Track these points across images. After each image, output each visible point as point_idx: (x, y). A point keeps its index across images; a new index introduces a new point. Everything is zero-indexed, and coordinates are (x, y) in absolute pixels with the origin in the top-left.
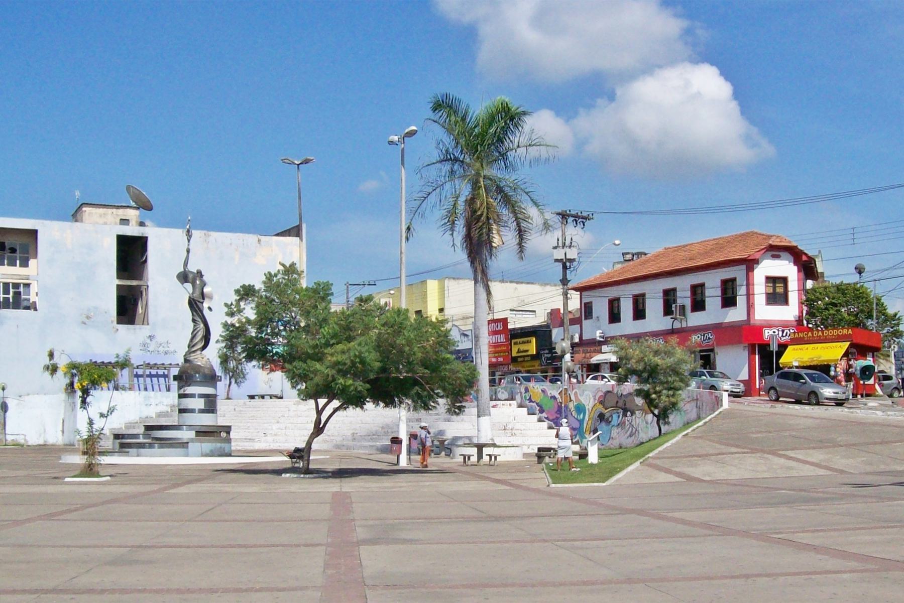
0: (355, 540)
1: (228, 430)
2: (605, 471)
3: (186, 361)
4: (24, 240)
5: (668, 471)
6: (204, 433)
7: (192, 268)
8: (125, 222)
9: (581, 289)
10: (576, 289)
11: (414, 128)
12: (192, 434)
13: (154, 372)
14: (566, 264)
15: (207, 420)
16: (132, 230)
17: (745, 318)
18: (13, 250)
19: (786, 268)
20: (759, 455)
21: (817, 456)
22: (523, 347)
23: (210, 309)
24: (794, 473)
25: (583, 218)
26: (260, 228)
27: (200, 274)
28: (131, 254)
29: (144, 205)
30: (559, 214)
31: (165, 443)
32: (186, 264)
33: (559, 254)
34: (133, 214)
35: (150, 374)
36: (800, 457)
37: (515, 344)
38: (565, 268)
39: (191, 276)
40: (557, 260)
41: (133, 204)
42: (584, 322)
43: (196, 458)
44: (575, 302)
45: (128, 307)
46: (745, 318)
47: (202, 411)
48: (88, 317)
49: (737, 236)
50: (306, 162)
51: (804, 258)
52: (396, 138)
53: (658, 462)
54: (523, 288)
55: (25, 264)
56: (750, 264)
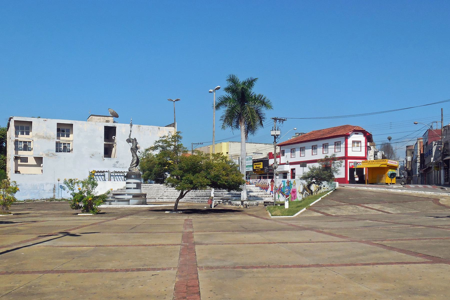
0: (193, 242)
1: (145, 195)
2: (291, 212)
3: (129, 170)
4: (68, 128)
5: (318, 212)
6: (135, 196)
7: (132, 137)
8: (107, 121)
9: (280, 146)
10: (278, 145)
11: (219, 86)
12: (131, 197)
13: (119, 174)
14: (275, 137)
15: (137, 192)
16: (110, 124)
17: (364, 156)
18: (63, 131)
19: (361, 138)
20: (353, 206)
21: (377, 207)
22: (258, 166)
23: (227, 153)
24: (369, 213)
25: (283, 120)
26: (159, 124)
27: (135, 140)
28: (110, 133)
29: (115, 115)
30: (273, 119)
31: (120, 200)
32: (130, 136)
33: (273, 133)
34: (111, 119)
35: (114, 175)
36: (370, 207)
37: (255, 165)
38: (275, 138)
39: (131, 140)
40: (272, 135)
41: (110, 115)
42: (281, 157)
43: (133, 205)
44: (278, 150)
45: (108, 152)
46: (364, 156)
47: (134, 188)
48: (93, 155)
49: (341, 127)
50: (177, 100)
51: (368, 134)
52: (212, 90)
53: (313, 208)
54: (258, 145)
55: (68, 136)
56: (347, 136)
